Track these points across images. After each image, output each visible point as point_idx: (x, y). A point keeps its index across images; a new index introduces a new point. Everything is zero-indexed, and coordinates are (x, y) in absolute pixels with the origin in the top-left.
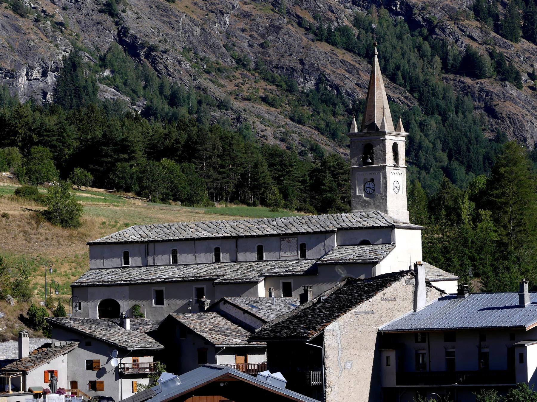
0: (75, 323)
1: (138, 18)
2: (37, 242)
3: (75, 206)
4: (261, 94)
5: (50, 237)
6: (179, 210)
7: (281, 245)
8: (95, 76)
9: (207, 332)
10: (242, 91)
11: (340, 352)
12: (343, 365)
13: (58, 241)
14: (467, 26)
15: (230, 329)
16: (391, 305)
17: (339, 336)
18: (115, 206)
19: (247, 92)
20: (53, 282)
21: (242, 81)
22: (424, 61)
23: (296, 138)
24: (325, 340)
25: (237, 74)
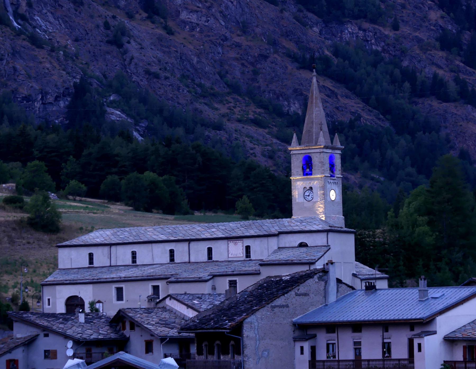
0: (35, 317)
1: (142, 48)
2: (20, 245)
3: (56, 213)
4: (251, 116)
5: (31, 241)
6: (151, 217)
7: (228, 247)
8: (103, 100)
9: (153, 325)
10: (234, 113)
11: (258, 342)
12: (260, 353)
13: (39, 245)
14: (433, 55)
15: (174, 322)
16: (305, 299)
17: (256, 328)
18: (94, 213)
19: (238, 115)
20: (32, 281)
21: (233, 105)
22: (395, 86)
23: (282, 156)
24: (244, 331)
25: (229, 98)
